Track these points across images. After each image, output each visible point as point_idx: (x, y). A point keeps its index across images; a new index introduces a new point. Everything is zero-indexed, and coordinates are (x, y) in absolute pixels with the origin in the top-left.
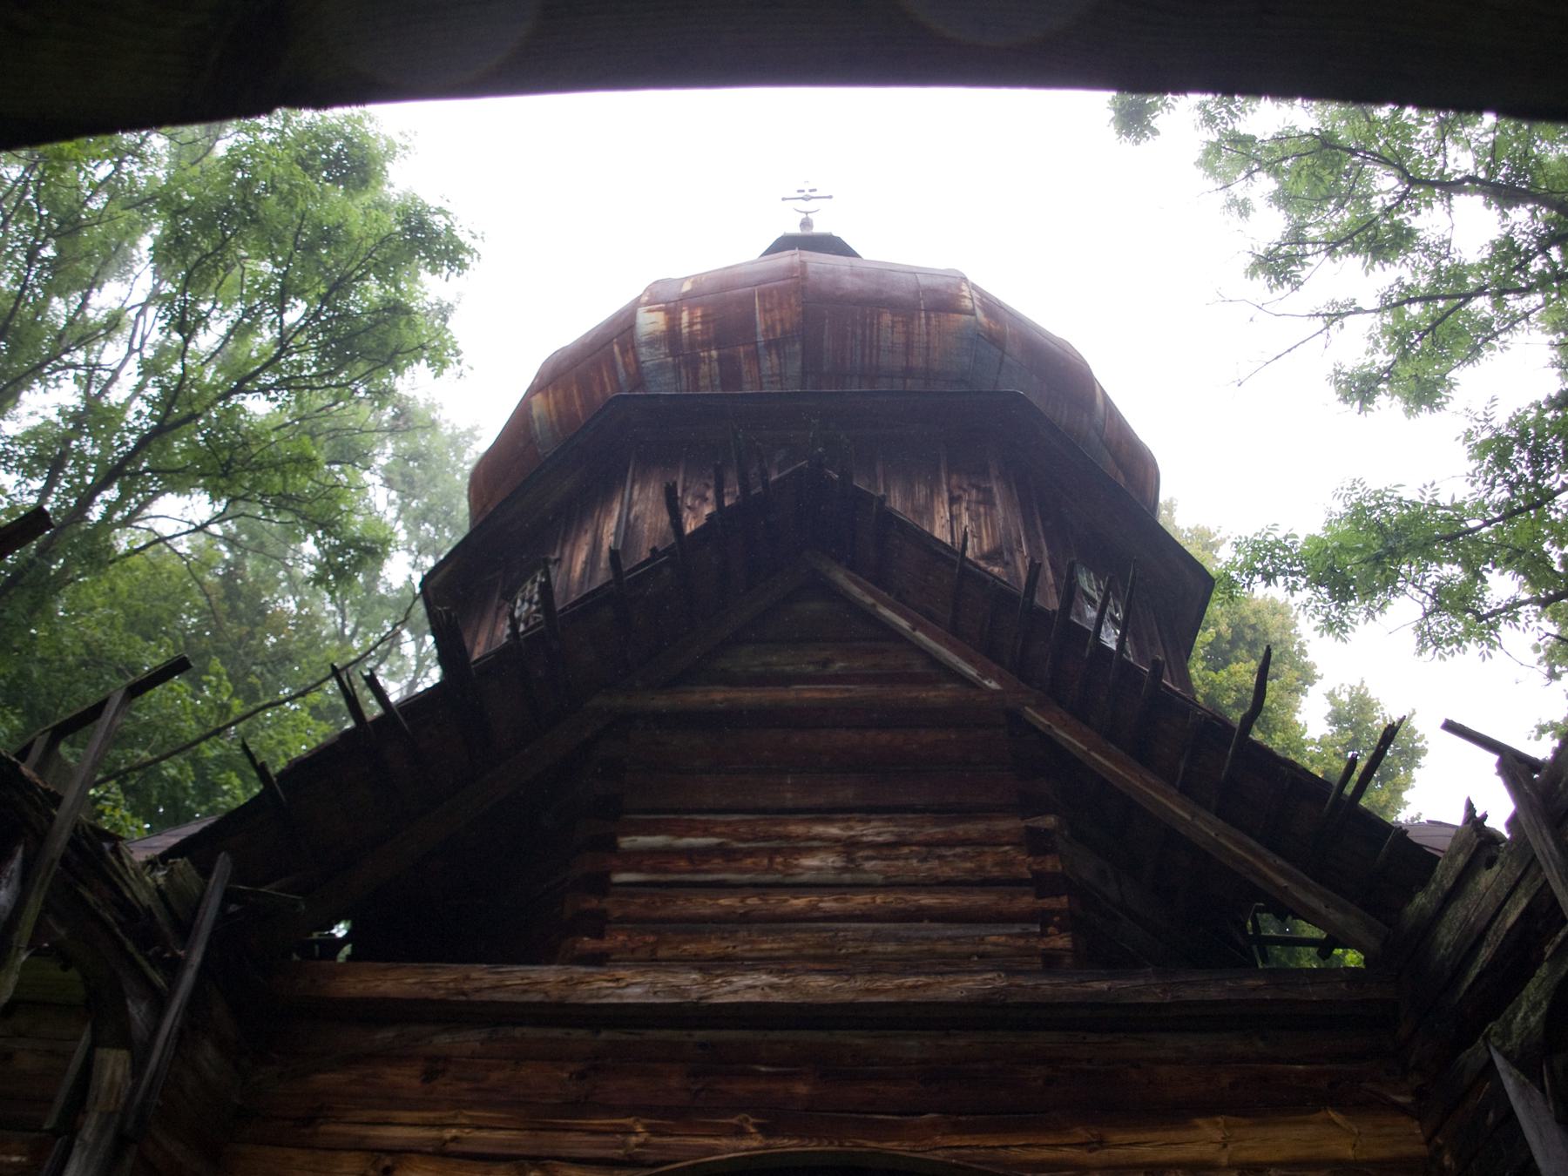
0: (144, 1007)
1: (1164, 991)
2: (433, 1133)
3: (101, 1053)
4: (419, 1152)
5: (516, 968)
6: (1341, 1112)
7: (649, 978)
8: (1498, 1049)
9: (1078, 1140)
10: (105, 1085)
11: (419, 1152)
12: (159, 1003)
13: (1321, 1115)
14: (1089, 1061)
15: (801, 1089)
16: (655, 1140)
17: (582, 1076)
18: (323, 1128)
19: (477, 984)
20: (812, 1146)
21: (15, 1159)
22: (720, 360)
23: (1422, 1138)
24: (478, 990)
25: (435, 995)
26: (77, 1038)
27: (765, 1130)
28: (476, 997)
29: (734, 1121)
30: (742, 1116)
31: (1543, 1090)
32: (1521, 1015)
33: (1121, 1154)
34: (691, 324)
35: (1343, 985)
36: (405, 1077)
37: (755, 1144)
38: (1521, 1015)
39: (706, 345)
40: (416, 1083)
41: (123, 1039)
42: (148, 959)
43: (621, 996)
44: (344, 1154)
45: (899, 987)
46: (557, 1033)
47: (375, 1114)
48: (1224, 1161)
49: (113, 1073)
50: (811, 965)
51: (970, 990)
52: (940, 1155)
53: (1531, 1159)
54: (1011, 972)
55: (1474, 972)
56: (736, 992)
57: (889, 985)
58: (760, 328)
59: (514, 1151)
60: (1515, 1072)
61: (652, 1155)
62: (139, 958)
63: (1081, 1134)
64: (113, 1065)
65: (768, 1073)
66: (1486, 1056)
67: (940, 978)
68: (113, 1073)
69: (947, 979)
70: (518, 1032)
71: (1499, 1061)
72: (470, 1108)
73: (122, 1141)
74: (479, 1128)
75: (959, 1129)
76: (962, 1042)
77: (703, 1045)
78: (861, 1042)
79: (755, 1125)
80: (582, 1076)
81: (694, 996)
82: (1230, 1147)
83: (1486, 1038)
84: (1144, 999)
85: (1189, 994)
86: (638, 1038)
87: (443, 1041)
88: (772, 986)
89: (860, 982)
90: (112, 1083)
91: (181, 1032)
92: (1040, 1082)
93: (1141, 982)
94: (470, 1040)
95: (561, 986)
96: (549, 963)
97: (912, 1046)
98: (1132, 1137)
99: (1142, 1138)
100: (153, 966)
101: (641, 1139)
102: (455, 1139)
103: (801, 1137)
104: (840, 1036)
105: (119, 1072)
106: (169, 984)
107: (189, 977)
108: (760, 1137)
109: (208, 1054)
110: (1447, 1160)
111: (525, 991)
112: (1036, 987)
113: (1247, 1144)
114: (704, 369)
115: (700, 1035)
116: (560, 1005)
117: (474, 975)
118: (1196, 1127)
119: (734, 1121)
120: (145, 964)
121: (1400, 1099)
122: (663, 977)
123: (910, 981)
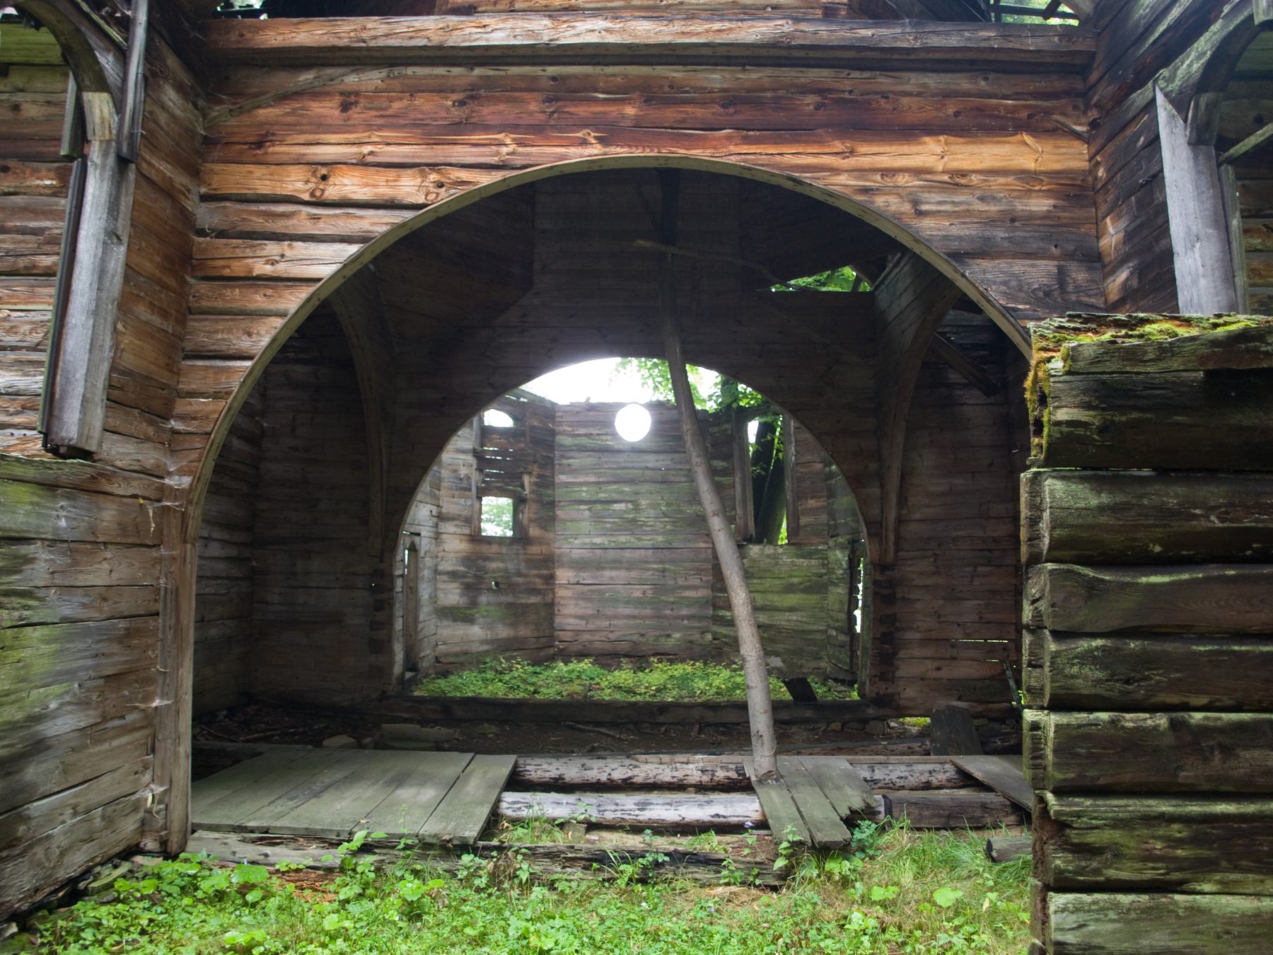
0: (111, 58)
1: (916, 39)
2: (354, 149)
3: (88, 96)
4: (345, 163)
5: (402, 19)
6: (1034, 137)
7: (510, 24)
8: (1161, 89)
9: (835, 150)
10: (98, 121)
11: (345, 163)
12: (123, 55)
13: (1018, 137)
14: (851, 92)
15: (630, 111)
16: (521, 150)
17: (462, 103)
18: (271, 150)
19: (373, 33)
20: (638, 153)
21: (48, 182)
23: (1087, 157)
24: (375, 38)
25: (341, 43)
26: (65, 91)
27: (601, 140)
28: (372, 44)
29: (580, 135)
30: (586, 131)
31: (1185, 121)
32: (1188, 62)
33: (865, 162)
35: (1056, 39)
36: (327, 109)
37: (596, 152)
38: (1188, 62)
40: (337, 113)
41: (101, 84)
42: (102, 17)
43: (487, 40)
44: (292, 167)
45: (707, 31)
46: (440, 71)
47: (311, 137)
48: (940, 168)
49: (101, 111)
50: (637, 14)
51: (763, 34)
52: (733, 160)
53: (1162, 170)
54: (797, 20)
55: (1161, 28)
56: (579, 35)
57: (700, 29)
59: (418, 161)
60: (1170, 107)
61: (519, 161)
62: (95, 17)
63: (838, 146)
64: (99, 106)
65: (605, 100)
66: (1151, 95)
67: (740, 24)
68: (101, 111)
69: (746, 24)
70: (410, 71)
71: (1160, 99)
72: (379, 130)
73: (123, 163)
74: (388, 144)
75: (747, 141)
76: (754, 76)
77: (554, 79)
78: (675, 75)
79: (595, 138)
80: (462, 103)
81: (545, 39)
82: (946, 158)
83: (1155, 81)
84: (899, 44)
85: (935, 41)
86: (503, 73)
87: (352, 80)
88: (607, 30)
89: (677, 27)
90: (103, 119)
91: (145, 78)
92: (811, 107)
93: (899, 30)
94: (373, 79)
95: (440, 32)
96: (429, 14)
97: (716, 78)
98: (875, 149)
99: (882, 150)
100: (108, 24)
101: (510, 149)
102: (371, 153)
103: (630, 146)
104: (661, 70)
105: (106, 111)
106: (126, 40)
107: (140, 33)
108: (599, 146)
109: (170, 96)
110: (1101, 172)
111: (411, 38)
112: (816, 33)
113: (959, 157)
115: (551, 70)
116: (440, 48)
117: (369, 26)
118: (925, 143)
119: (580, 135)
120: (102, 22)
121: (1078, 128)
122: (520, 23)
123: (717, 26)
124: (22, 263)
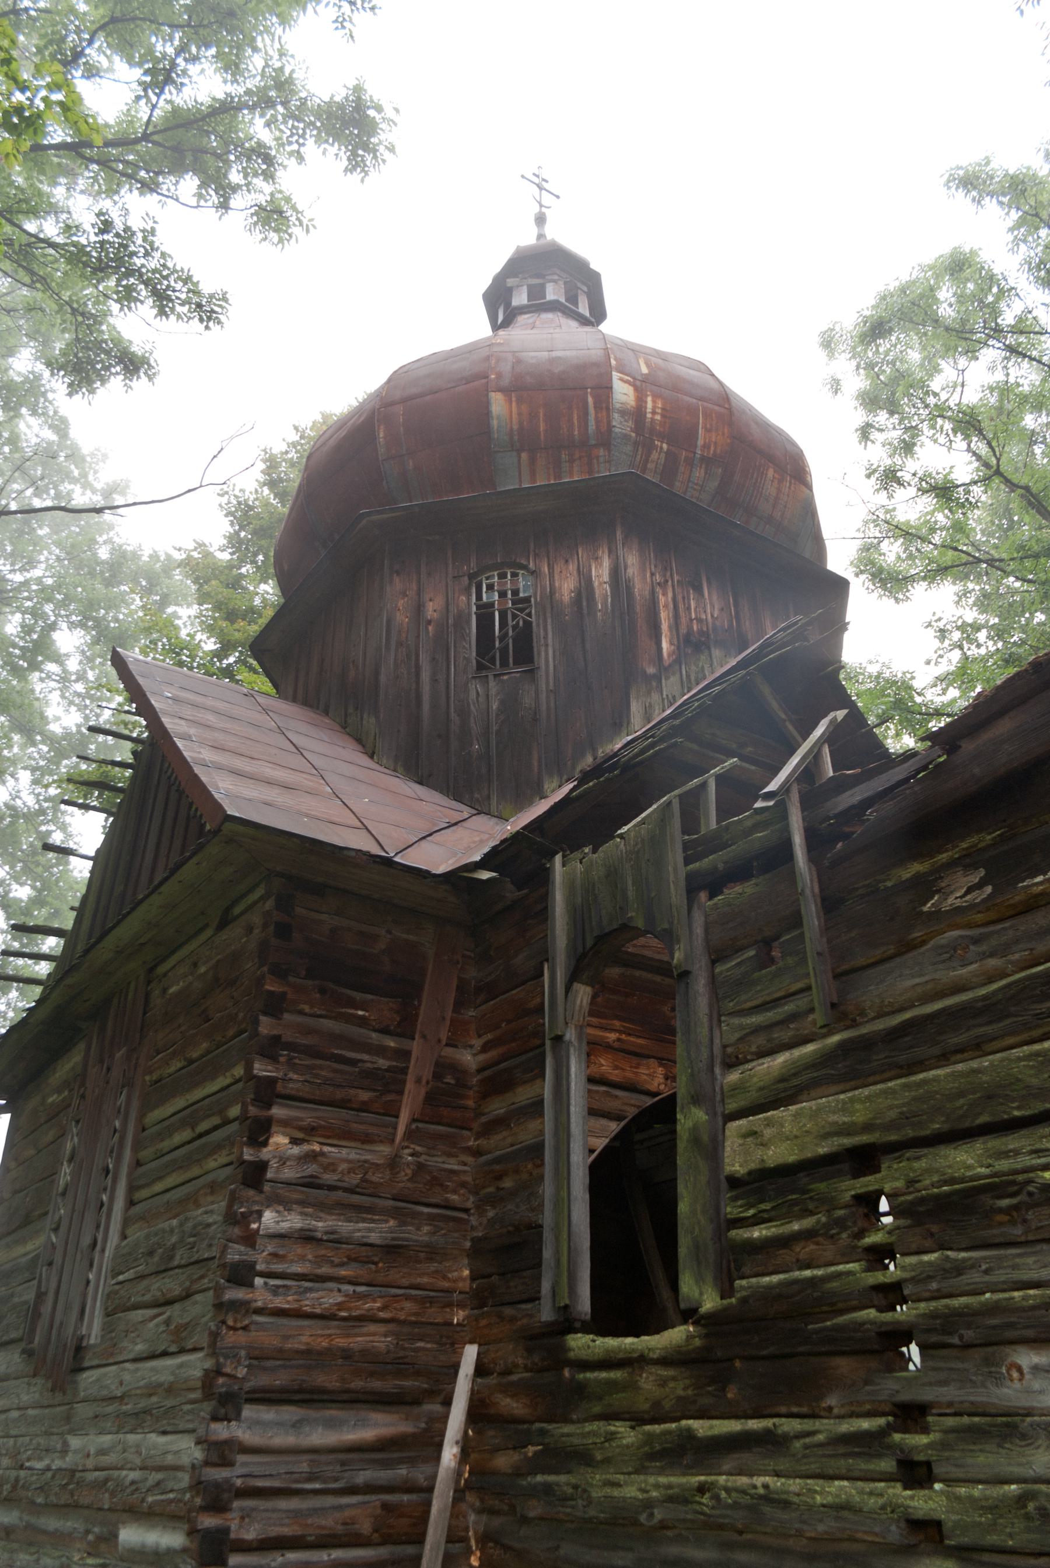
22: (668, 453)
34: (654, 413)
39: (662, 437)
58: (700, 442)
114: (654, 455)
124: (339, 1094)
